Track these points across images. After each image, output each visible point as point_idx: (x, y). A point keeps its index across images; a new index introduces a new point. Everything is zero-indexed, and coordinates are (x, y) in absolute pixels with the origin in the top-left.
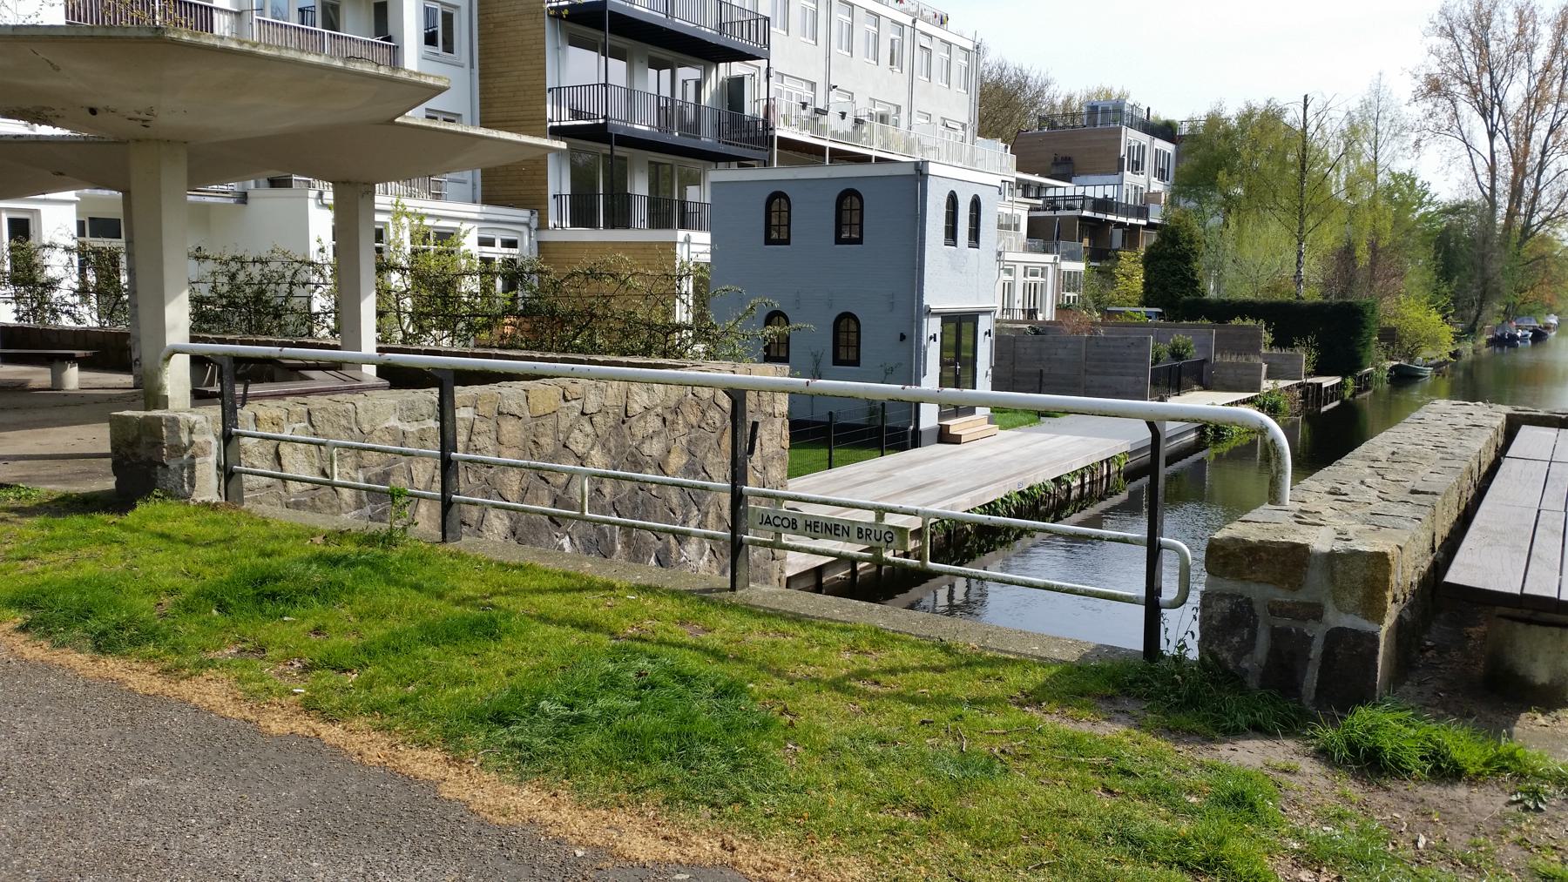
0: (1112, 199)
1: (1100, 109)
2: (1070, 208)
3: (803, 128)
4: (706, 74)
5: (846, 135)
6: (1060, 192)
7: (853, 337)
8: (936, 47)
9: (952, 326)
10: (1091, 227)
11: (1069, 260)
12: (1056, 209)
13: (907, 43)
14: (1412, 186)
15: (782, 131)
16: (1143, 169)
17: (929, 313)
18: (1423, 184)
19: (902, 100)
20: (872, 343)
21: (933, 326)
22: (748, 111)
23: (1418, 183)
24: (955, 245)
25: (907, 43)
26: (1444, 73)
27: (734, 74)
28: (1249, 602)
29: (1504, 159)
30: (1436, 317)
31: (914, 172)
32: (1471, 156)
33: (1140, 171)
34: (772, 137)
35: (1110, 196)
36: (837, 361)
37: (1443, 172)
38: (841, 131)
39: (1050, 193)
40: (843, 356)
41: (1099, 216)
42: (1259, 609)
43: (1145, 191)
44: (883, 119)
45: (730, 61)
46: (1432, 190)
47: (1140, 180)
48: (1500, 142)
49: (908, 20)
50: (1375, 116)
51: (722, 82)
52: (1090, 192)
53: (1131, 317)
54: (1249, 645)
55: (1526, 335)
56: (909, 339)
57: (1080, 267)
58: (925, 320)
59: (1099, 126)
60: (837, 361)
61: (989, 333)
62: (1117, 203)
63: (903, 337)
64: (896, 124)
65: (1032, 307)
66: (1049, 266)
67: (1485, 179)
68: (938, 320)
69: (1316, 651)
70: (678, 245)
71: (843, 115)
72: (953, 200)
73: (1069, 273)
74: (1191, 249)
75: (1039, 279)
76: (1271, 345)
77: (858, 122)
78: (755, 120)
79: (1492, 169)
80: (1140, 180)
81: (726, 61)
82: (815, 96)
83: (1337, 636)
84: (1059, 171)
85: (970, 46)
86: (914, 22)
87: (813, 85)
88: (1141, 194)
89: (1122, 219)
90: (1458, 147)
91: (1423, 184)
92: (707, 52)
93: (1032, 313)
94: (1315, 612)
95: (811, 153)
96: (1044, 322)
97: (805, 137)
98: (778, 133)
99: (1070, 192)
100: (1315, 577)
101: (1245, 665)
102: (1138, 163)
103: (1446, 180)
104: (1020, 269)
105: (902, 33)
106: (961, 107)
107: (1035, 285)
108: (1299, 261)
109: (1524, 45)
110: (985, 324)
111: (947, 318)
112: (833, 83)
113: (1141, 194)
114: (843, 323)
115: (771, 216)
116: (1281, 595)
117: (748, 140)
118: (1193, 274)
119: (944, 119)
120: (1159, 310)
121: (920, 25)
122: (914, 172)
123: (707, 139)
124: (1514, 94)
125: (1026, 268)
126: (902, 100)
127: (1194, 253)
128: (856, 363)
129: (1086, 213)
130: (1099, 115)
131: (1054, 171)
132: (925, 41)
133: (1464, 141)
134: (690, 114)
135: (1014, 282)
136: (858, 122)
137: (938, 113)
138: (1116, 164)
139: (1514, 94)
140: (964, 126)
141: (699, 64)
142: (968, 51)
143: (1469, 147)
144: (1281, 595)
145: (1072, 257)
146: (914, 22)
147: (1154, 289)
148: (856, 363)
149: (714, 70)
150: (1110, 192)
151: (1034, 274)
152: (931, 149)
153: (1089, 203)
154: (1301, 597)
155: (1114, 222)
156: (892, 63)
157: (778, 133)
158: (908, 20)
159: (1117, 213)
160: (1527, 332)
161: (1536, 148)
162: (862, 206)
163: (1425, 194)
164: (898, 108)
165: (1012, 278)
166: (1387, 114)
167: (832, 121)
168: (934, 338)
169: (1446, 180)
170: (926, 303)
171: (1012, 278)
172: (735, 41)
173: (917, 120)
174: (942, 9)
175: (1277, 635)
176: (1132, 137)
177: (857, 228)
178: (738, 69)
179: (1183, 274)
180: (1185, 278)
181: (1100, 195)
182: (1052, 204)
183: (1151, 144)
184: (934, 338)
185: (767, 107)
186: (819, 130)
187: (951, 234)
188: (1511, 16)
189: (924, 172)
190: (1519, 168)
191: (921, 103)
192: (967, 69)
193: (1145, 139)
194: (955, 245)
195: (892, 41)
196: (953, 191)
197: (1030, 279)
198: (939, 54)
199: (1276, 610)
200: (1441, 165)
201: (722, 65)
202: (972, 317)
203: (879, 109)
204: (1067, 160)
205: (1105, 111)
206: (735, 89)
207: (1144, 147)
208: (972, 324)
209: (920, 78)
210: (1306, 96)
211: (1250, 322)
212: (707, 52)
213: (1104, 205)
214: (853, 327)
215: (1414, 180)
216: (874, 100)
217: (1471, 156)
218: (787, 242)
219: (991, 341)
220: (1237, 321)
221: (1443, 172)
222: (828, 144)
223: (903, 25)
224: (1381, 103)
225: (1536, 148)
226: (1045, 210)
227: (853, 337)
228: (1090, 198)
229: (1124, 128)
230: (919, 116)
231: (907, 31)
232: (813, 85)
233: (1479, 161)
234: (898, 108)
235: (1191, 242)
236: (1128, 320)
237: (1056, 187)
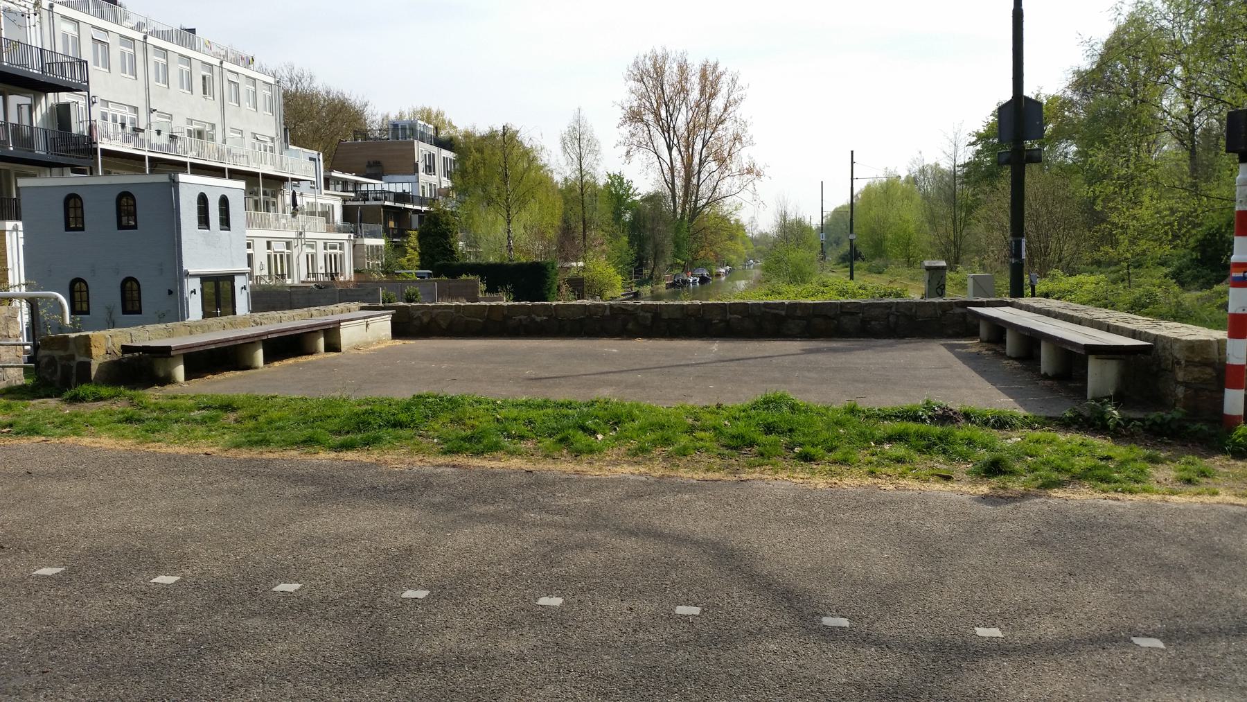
0: (409, 193)
1: (400, 127)
2: (376, 199)
3: (125, 140)
4: (36, 101)
5: (163, 147)
6: (371, 188)
7: (135, 294)
8: (241, 81)
9: (212, 284)
10: (394, 213)
11: (371, 237)
12: (366, 199)
13: (217, 78)
14: (621, 183)
15: (104, 144)
16: (434, 171)
17: (188, 275)
18: (628, 182)
19: (216, 120)
20: (150, 297)
21: (193, 284)
22: (75, 130)
23: (625, 181)
24: (209, 228)
25: (217, 78)
26: (639, 106)
27: (62, 101)
28: (54, 357)
29: (678, 165)
30: (612, 270)
31: (168, 181)
32: (660, 163)
33: (432, 173)
34: (96, 149)
35: (407, 191)
36: (125, 312)
37: (644, 173)
38: (159, 143)
39: (364, 188)
40: (129, 307)
41: (398, 205)
42: (57, 359)
43: (438, 187)
44: (200, 134)
45: (58, 92)
46: (634, 186)
47: (434, 179)
48: (675, 152)
49: (216, 62)
50: (578, 137)
51: (52, 107)
52: (392, 188)
53: (405, 277)
54: (55, 372)
55: (696, 280)
56: (175, 294)
57: (381, 242)
58: (186, 280)
59: (400, 140)
60: (125, 312)
61: (244, 288)
62: (413, 196)
63: (170, 292)
64: (212, 139)
65: (334, 272)
66: (345, 242)
67: (669, 177)
68: (198, 280)
69: (74, 371)
70: (7, 233)
71: (159, 132)
72: (203, 200)
73: (372, 246)
74: (448, 229)
75: (338, 251)
76: (485, 292)
77: (173, 137)
78: (81, 136)
79: (672, 169)
80: (434, 179)
81: (54, 92)
82: (138, 117)
83: (80, 364)
84: (372, 171)
85: (272, 81)
86: (221, 63)
87: (136, 109)
88: (435, 190)
89: (419, 208)
90: (652, 156)
91: (628, 182)
92: (36, 87)
93: (333, 276)
94: (72, 357)
95: (132, 162)
96: (345, 283)
97: (128, 148)
98: (100, 146)
99: (378, 188)
100: (72, 346)
101: (54, 379)
102: (430, 167)
103: (646, 179)
104: (320, 245)
105: (212, 71)
106: (268, 124)
107: (335, 256)
108: (509, 236)
109: (683, 91)
110: (239, 282)
111: (205, 279)
112: (153, 107)
113: (435, 190)
114: (128, 285)
115: (68, 211)
116: (62, 353)
117: (77, 151)
118: (451, 246)
119: (255, 134)
120: (431, 272)
121: (225, 65)
122: (168, 181)
123: (40, 150)
124: (681, 121)
125: (325, 243)
126: (216, 120)
127: (450, 232)
128: (139, 312)
129: (387, 203)
130: (400, 132)
131: (368, 171)
132: (233, 78)
133: (656, 153)
134: (26, 131)
135: (316, 254)
136: (173, 137)
137: (249, 129)
138: (412, 168)
139: (681, 121)
140: (272, 139)
141: (30, 95)
142: (271, 85)
143: (658, 157)
144: (62, 353)
145: (374, 235)
146: (221, 63)
147: (426, 257)
148: (139, 312)
149: (44, 98)
150: (407, 188)
151: (334, 248)
152: (242, 156)
153: (392, 196)
154: (68, 353)
155: (411, 209)
156: (205, 93)
157: (100, 146)
158: (216, 62)
159: (413, 203)
160: (696, 278)
161: (696, 160)
162: (82, 204)
163: (630, 189)
164: (213, 126)
165: (314, 251)
166: (585, 136)
167: (150, 136)
168: (194, 292)
169: (646, 179)
170: (185, 268)
171: (314, 251)
172: (55, 76)
173: (229, 134)
174: (248, 53)
175: (63, 366)
176: (422, 149)
177: (80, 220)
178: (64, 97)
179: (443, 246)
180: (445, 249)
181: (400, 190)
182: (365, 196)
183: (439, 153)
184: (194, 292)
185: (91, 126)
186: (139, 144)
187: (204, 221)
188: (675, 69)
189: (176, 180)
190: (688, 166)
191: (232, 122)
192: (271, 98)
193: (434, 150)
194: (209, 228)
195: (204, 78)
196: (202, 193)
197: (329, 251)
198: (245, 87)
199: (61, 358)
200: (642, 169)
201: (50, 95)
202: (230, 278)
203: (196, 127)
204: (377, 164)
205: (404, 129)
206: (62, 114)
207: (434, 155)
208: (229, 283)
209: (231, 105)
210: (852, 152)
211: (471, 277)
212: (36, 87)
213: (402, 197)
214: (135, 286)
215: (622, 179)
216: (192, 120)
217: (660, 163)
218: (82, 229)
219: (248, 293)
220: (464, 277)
221: (644, 173)
222: (147, 154)
223: (212, 65)
224: (581, 129)
225: (696, 160)
226: (358, 201)
227: (135, 294)
228: (392, 192)
229: (416, 142)
230: (231, 131)
231: (216, 70)
232: (136, 109)
233: (665, 166)
234: (213, 126)
235: (447, 224)
236: (404, 279)
237: (368, 183)
